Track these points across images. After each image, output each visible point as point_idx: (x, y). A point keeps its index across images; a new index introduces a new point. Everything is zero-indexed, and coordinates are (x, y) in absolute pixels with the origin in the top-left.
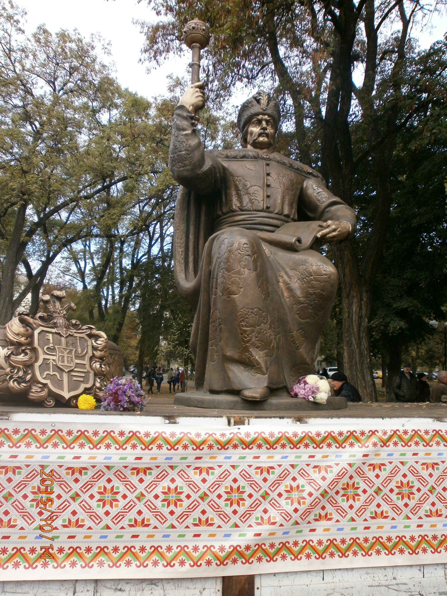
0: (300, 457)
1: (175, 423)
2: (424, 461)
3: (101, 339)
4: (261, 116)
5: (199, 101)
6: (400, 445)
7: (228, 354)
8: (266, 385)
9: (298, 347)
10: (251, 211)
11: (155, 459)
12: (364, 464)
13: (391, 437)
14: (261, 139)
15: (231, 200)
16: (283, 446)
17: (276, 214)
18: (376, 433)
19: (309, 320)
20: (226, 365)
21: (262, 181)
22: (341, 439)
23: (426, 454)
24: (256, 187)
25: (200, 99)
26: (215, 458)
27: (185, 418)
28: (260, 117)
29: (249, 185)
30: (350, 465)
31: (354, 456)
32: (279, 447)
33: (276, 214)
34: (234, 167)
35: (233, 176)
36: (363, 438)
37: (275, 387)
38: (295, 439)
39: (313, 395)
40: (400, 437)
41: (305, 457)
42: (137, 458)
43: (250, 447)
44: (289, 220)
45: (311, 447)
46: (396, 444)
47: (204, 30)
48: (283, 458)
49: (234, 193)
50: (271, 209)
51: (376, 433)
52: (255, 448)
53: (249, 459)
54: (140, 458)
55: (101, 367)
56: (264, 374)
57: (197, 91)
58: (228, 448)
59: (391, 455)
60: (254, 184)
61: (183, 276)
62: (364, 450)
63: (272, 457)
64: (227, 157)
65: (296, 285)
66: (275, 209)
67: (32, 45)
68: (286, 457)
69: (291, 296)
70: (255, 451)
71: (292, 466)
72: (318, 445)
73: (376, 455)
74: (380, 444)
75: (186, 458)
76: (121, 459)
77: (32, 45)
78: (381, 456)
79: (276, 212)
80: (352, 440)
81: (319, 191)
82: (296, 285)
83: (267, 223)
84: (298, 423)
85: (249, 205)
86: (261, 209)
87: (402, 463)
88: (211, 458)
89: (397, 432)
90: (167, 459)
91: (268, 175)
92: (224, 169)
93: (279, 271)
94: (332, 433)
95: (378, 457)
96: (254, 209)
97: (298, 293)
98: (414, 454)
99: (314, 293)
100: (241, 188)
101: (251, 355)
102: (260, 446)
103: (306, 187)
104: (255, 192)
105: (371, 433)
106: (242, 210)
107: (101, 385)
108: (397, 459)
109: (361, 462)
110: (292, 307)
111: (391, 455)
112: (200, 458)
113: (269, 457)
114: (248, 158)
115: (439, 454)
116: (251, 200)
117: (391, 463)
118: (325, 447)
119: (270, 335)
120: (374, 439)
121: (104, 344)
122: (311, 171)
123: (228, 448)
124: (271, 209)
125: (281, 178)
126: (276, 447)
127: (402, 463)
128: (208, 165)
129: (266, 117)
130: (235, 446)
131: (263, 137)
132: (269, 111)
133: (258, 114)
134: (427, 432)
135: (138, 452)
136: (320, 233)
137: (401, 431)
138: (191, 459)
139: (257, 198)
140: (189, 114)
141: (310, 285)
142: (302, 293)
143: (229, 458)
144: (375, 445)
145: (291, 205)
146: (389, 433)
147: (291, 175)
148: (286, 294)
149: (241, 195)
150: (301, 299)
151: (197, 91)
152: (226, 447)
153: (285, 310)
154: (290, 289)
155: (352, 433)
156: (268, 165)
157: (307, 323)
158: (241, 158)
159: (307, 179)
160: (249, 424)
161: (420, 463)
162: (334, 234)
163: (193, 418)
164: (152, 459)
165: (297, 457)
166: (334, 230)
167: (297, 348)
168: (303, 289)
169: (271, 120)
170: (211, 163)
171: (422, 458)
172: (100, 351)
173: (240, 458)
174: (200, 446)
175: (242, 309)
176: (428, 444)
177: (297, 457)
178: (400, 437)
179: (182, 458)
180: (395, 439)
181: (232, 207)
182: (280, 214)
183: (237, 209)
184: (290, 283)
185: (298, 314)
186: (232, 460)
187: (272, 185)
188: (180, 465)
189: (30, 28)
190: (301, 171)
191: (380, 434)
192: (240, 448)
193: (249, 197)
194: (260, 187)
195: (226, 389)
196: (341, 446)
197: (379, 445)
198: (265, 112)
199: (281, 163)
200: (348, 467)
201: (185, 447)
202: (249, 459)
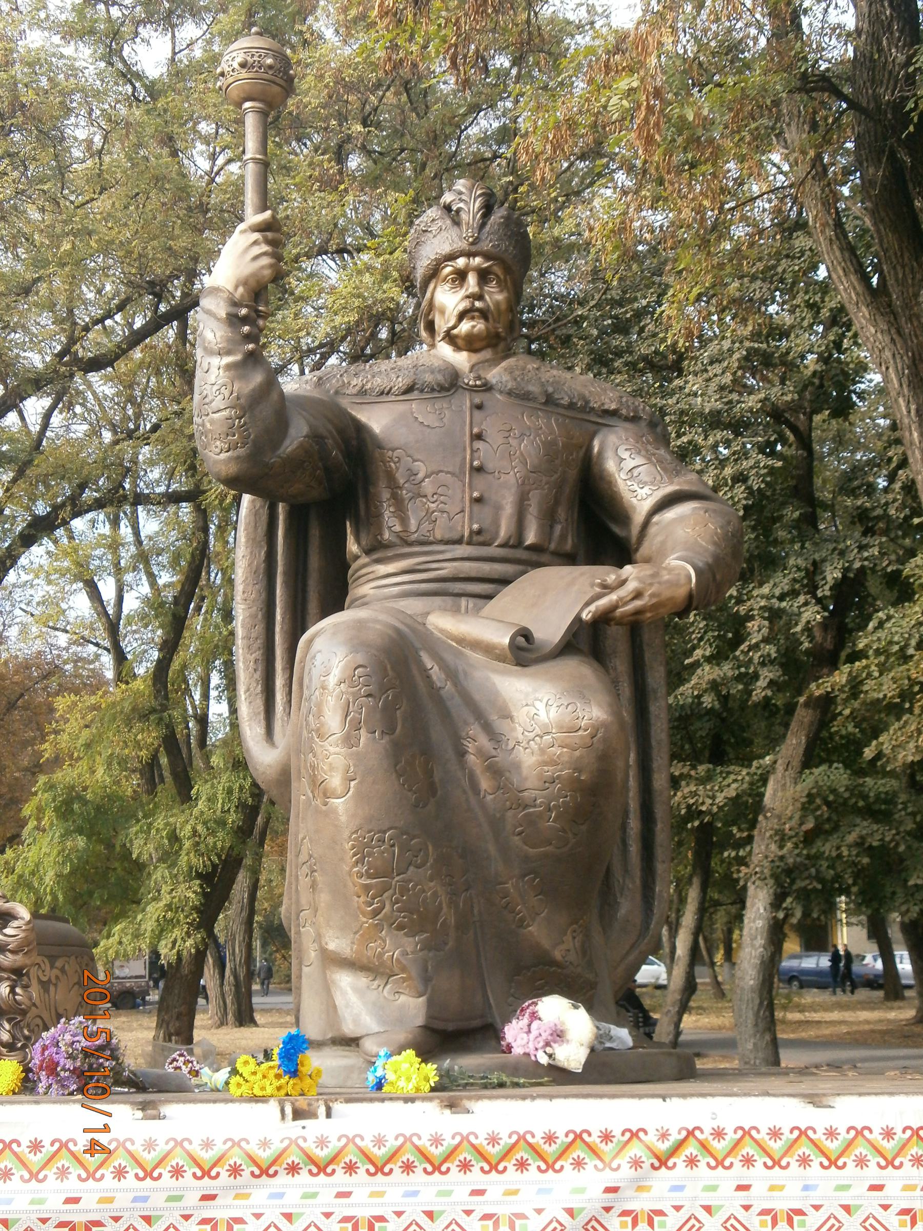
0: (449, 1193)
1: (159, 1117)
2: (768, 1205)
3: (15, 923)
5: (262, 267)
6: (702, 1164)
7: (332, 946)
9: (522, 920)
10: (431, 543)
11: (111, 1200)
12: (608, 1209)
13: (680, 1145)
15: (379, 515)
16: (408, 1167)
18: (641, 1134)
19: (549, 848)
20: (328, 973)
21: (458, 460)
22: (551, 1150)
23: (772, 1188)
25: (265, 261)
26: (247, 1196)
27: (181, 1106)
28: (461, 262)
30: (570, 1212)
31: (582, 1190)
32: (397, 1171)
36: (607, 1149)
37: (451, 1027)
38: (437, 1152)
39: (548, 1050)
40: (703, 1145)
41: (461, 1195)
42: (68, 1201)
43: (329, 1170)
44: (544, 558)
45: (476, 1169)
46: (692, 1162)
48: (408, 1194)
49: (386, 495)
51: (641, 1134)
52: (340, 1172)
53: (326, 1199)
54: (76, 1200)
55: (12, 991)
57: (255, 243)
58: (276, 1173)
59: (679, 1188)
61: (260, 730)
62: (609, 1178)
63: (381, 1194)
68: (415, 1193)
69: (499, 788)
70: (341, 1180)
71: (430, 1215)
72: (494, 1167)
73: (640, 1189)
74: (648, 1160)
75: (179, 1198)
76: (32, 1202)
78: (654, 1192)
80: (579, 1152)
83: (473, 574)
84: (447, 1112)
87: (708, 1209)
88: (237, 1196)
89: (697, 1133)
90: (135, 1200)
91: (479, 437)
93: (466, 723)
94: (529, 1137)
95: (645, 1195)
98: (740, 1188)
100: (402, 481)
102: (351, 1168)
103: (600, 452)
105: (628, 1135)
107: (14, 1037)
108: (695, 1198)
109: (599, 1206)
111: (679, 1188)
112: (212, 1197)
113: (373, 1194)
115: (806, 1188)
117: (678, 1208)
118: (511, 1168)
119: (435, 894)
120: (636, 1150)
121: (22, 935)
123: (276, 1173)
125: (514, 442)
126: (391, 1170)
127: (708, 1209)
128: (298, 432)
129: (478, 260)
130: (293, 1169)
131: (473, 318)
132: (486, 245)
133: (452, 257)
134: (775, 1134)
135: (72, 1185)
136: (592, 608)
137: (708, 1130)
138: (192, 1199)
143: (281, 1195)
144: (636, 1163)
145: (549, 518)
146: (675, 1137)
147: (548, 426)
148: (485, 784)
149: (403, 500)
152: (271, 1172)
155: (578, 1136)
156: (479, 407)
159: (605, 430)
160: (329, 1115)
161: (756, 1209)
162: (638, 603)
163: (200, 1105)
164: (102, 1201)
165: (441, 1194)
166: (638, 595)
167: (521, 923)
169: (496, 269)
170: (305, 430)
171: (760, 1197)
172: (13, 952)
173: (306, 1196)
174: (212, 1168)
176: (776, 1163)
177: (441, 1194)
178: (703, 1145)
179: (170, 1199)
180: (691, 1149)
181: (381, 535)
182: (513, 547)
183: (393, 539)
184: (494, 753)
185: (520, 834)
186: (286, 1200)
187: (490, 466)
188: (166, 1214)
191: (651, 1138)
192: (304, 1173)
194: (453, 474)
195: (329, 1036)
196: (550, 1166)
197: (646, 1166)
199: (518, 396)
200: (565, 1218)
201: (177, 1172)
202: (326, 1199)
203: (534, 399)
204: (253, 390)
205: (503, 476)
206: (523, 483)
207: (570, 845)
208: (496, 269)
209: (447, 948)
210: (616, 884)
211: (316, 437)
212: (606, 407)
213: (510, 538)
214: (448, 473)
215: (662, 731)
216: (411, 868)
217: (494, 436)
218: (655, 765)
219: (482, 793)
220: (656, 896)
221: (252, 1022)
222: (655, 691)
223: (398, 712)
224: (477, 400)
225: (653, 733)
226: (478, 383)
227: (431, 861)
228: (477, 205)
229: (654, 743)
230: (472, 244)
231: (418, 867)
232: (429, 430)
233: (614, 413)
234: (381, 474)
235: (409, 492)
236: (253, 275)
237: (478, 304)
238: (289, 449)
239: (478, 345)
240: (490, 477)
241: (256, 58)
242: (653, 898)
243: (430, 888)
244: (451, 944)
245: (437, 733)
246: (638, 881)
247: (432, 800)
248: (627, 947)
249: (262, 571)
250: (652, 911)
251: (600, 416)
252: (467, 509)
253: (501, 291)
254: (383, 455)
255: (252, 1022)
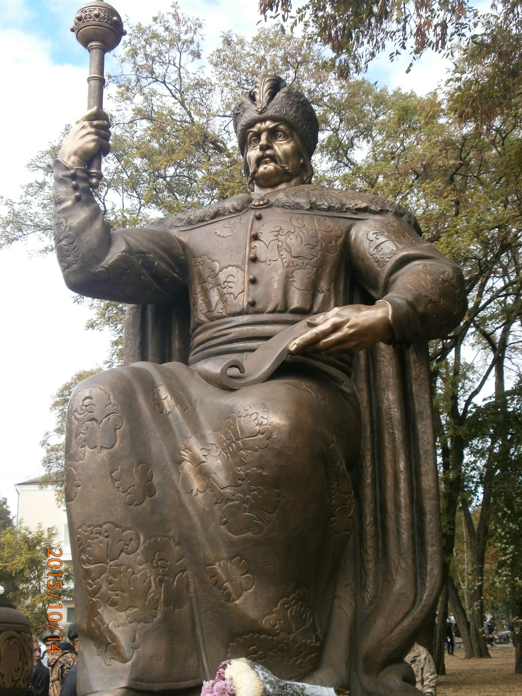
4: (259, 125)
5: (87, 142)
8: (124, 683)
10: (224, 317)
14: (261, 169)
17: (273, 311)
19: (250, 534)
24: (230, 268)
29: (217, 265)
33: (273, 311)
34: (198, 239)
35: (194, 257)
47: (97, 16)
49: (199, 289)
50: (259, 306)
56: (124, 660)
57: (83, 127)
60: (225, 264)
64: (190, 222)
65: (215, 462)
66: (268, 303)
67: (209, 73)
77: (209, 73)
79: (270, 308)
81: (379, 242)
82: (215, 462)
83: (250, 335)
85: (221, 306)
86: (238, 309)
91: (255, 237)
92: (184, 246)
96: (228, 312)
97: (221, 478)
99: (247, 475)
101: (102, 620)
103: (355, 239)
104: (229, 280)
106: (211, 319)
110: (211, 509)
114: (224, 215)
116: (222, 295)
119: (145, 576)
122: (364, 205)
124: (259, 306)
131: (266, 163)
139: (232, 290)
140: (68, 173)
141: (237, 460)
142: (227, 478)
148: (196, 485)
150: (228, 490)
151: (83, 127)
153: (190, 518)
154: (203, 473)
157: (247, 540)
158: (213, 218)
159: (359, 223)
167: (229, 598)
168: (228, 468)
170: (123, 247)
175: (81, 527)
182: (280, 312)
184: (203, 459)
185: (225, 523)
187: (262, 257)
189: (210, 44)
190: (340, 210)
193: (219, 290)
194: (237, 266)
198: (264, 115)
203: (301, 208)
204: (79, 223)
205: (272, 262)
206: (288, 266)
207: (265, 531)
208: (282, 127)
209: (155, 620)
210: (393, 564)
211: (130, 250)
212: (359, 206)
213: (277, 306)
214: (233, 266)
215: (428, 443)
216: (123, 554)
217: (266, 235)
218: (423, 469)
219: (195, 492)
220: (428, 573)
221: (488, 656)
222: (421, 413)
223: (118, 431)
224: (257, 214)
225: (420, 445)
226: (261, 203)
227: (141, 548)
228: (266, 87)
229: (422, 453)
230: (261, 113)
231: (128, 554)
232: (222, 239)
233: (365, 210)
234: (196, 276)
235: (210, 283)
236: (80, 148)
237: (268, 152)
238: (110, 262)
239: (273, 181)
240: (263, 264)
241: (88, 13)
242: (426, 575)
243: (139, 571)
244: (159, 616)
245: (157, 445)
246: (410, 561)
247: (147, 498)
248: (401, 615)
249: (137, 355)
250: (425, 585)
251: (355, 214)
252: (246, 289)
253: (289, 142)
254: (195, 261)
255: (488, 656)
